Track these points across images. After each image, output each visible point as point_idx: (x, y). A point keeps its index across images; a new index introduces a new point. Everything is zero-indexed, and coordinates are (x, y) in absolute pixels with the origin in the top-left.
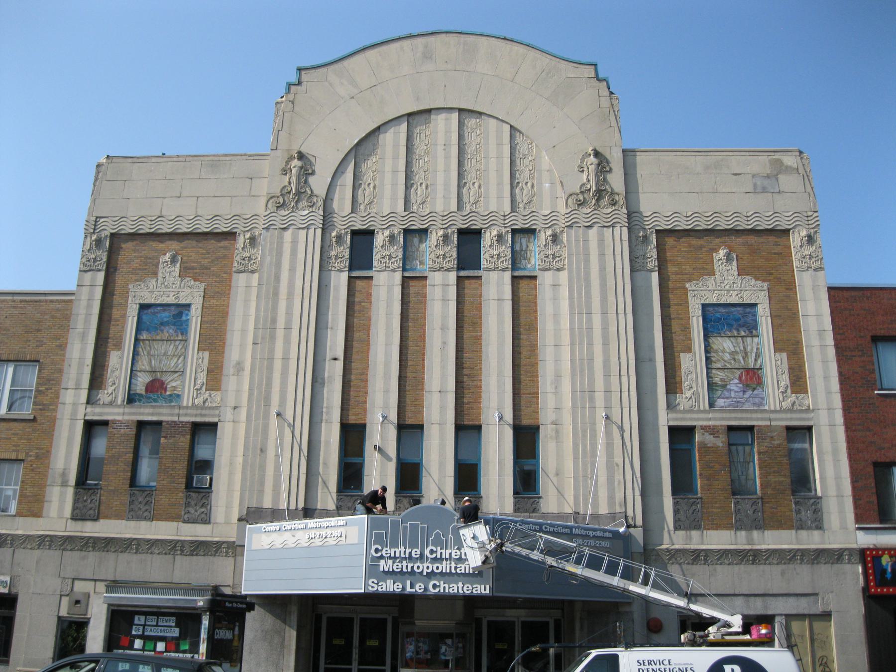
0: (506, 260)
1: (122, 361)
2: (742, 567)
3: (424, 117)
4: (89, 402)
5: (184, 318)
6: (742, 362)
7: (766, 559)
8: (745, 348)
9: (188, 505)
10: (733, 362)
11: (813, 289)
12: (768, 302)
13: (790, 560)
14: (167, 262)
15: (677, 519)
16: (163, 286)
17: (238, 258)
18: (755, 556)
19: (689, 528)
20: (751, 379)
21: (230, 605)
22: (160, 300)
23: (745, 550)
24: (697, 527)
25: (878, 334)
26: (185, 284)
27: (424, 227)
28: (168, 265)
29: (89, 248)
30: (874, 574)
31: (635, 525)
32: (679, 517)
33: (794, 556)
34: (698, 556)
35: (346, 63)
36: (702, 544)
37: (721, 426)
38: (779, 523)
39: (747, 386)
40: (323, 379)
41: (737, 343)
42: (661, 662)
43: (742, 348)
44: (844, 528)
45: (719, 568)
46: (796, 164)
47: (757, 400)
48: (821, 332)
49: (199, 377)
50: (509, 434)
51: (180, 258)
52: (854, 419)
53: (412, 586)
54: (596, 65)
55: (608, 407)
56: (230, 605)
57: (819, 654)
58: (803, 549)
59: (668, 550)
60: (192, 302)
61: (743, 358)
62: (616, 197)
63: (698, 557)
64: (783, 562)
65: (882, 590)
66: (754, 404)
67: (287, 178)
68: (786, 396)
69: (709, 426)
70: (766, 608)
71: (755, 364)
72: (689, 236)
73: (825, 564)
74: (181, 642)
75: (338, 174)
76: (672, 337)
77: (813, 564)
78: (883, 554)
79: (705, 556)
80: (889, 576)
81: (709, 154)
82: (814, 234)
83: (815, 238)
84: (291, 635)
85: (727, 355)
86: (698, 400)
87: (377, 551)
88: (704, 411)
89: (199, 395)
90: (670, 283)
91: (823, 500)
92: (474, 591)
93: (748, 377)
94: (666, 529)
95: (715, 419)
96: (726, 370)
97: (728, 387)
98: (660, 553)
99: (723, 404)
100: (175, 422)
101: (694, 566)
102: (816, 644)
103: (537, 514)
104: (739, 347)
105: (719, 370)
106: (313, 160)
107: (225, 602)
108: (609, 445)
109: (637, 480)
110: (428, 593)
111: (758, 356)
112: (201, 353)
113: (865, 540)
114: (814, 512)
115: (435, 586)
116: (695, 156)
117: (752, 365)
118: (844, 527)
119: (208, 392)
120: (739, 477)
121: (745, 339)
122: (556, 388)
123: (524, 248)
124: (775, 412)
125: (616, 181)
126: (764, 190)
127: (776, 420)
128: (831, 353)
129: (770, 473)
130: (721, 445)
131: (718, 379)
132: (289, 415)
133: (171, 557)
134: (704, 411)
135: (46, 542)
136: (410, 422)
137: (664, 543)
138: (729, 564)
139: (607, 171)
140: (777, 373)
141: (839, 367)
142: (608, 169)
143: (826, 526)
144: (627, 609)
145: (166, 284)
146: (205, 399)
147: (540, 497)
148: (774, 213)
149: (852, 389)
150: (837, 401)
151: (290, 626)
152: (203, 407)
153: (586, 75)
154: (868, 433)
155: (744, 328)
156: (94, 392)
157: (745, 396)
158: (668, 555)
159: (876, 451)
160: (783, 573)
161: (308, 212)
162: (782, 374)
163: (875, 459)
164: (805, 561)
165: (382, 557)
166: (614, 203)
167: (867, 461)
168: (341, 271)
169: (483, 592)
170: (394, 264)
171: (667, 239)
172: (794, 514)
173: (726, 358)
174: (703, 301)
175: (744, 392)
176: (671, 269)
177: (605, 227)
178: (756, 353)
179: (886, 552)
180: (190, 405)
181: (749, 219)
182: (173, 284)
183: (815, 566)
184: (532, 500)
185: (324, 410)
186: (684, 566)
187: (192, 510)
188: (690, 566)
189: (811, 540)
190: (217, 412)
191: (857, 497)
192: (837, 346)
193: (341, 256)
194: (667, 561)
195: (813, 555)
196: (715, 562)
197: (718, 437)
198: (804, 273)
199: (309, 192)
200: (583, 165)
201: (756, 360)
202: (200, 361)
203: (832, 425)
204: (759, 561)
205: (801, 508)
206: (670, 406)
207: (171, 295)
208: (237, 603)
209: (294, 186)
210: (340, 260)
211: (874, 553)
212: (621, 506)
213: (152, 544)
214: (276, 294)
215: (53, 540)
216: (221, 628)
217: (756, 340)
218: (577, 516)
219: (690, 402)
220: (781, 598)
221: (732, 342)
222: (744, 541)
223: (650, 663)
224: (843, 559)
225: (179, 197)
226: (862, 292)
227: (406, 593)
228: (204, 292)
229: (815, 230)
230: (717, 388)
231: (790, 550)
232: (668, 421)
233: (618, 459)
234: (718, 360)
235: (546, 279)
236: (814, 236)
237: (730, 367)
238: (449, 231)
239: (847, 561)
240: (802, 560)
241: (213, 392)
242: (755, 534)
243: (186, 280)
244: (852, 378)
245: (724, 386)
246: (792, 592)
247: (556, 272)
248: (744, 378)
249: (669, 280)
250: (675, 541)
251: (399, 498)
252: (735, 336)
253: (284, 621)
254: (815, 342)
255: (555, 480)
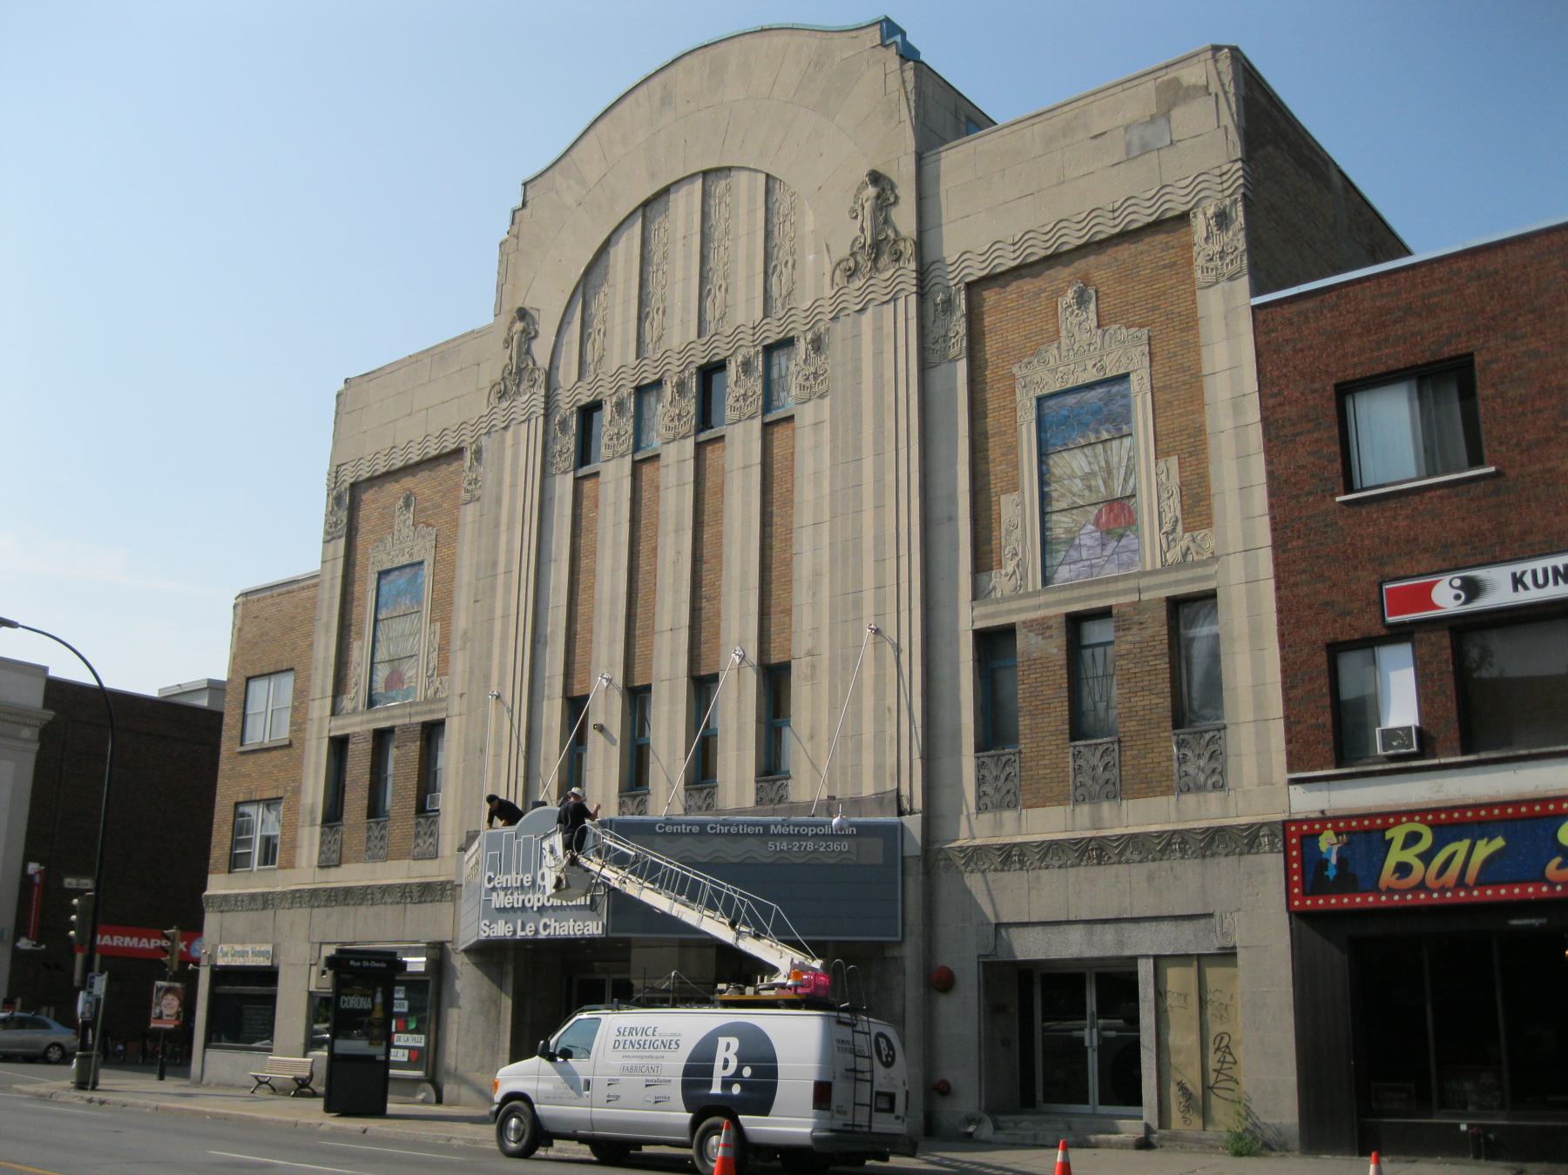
0: (1236, 257)
1: (363, 653)
2: (1081, 870)
3: (726, 172)
4: (335, 712)
5: (419, 581)
6: (1102, 489)
7: (1121, 854)
8: (1107, 462)
9: (417, 835)
10: (1086, 493)
11: (1225, 318)
12: (1148, 364)
13: (1163, 851)
14: (1070, 306)
15: (982, 794)
16: (1071, 353)
17: (1200, 261)
18: (1101, 849)
19: (1001, 806)
20: (1116, 517)
21: (358, 964)
22: (1071, 381)
23: (1083, 839)
24: (1012, 805)
25: (1349, 378)
26: (1111, 338)
27: (657, 376)
28: (1073, 312)
29: (1205, 235)
30: (1303, 871)
31: (911, 810)
32: (1082, 779)
33: (1169, 844)
34: (1009, 856)
35: (574, 153)
36: (1019, 833)
37: (1055, 616)
38: (1149, 786)
39: (1109, 532)
40: (546, 636)
41: (1096, 456)
42: (644, 1031)
43: (1103, 464)
44: (1265, 784)
45: (1044, 874)
46: (1204, 78)
47: (1124, 557)
48: (1237, 403)
49: (1167, 509)
50: (752, 679)
51: (1092, 292)
52: (1294, 562)
53: (523, 929)
54: (525, 184)
55: (879, 615)
56: (358, 964)
57: (1215, 1028)
58: (1182, 830)
59: (962, 849)
60: (1130, 368)
61: (1105, 482)
62: (901, 246)
63: (1010, 856)
64: (1150, 856)
65: (1327, 902)
66: (1120, 565)
67: (509, 351)
68: (1173, 540)
69: (1036, 620)
70: (1121, 944)
71: (1124, 489)
72: (1022, 277)
73: (1226, 855)
74: (409, 1019)
75: (565, 327)
76: (988, 469)
77: (1204, 856)
78: (1324, 828)
79: (1019, 855)
80: (1331, 873)
81: (1056, 112)
82: (1231, 206)
83: (1234, 215)
84: (507, 1003)
85: (1078, 481)
86: (1024, 577)
87: (490, 880)
88: (1036, 594)
89: (1172, 544)
90: (987, 373)
91: (1228, 731)
92: (586, 933)
93: (1112, 515)
94: (965, 813)
95: (1047, 605)
96: (1074, 511)
97: (1077, 541)
98: (951, 856)
99: (1067, 575)
100: (405, 725)
101: (1006, 874)
102: (1210, 1011)
103: (786, 805)
104: (1098, 463)
105: (1063, 513)
106: (536, 316)
107: (349, 960)
108: (879, 679)
109: (916, 732)
110: (540, 937)
111: (1130, 471)
112: (1162, 463)
113: (1307, 802)
114: (1211, 757)
115: (546, 926)
116: (1032, 125)
117: (1118, 493)
118: (1265, 781)
119: (1187, 535)
120: (1095, 706)
121: (1108, 444)
122: (814, 595)
123: (783, 374)
124: (1154, 572)
125: (904, 218)
126: (1146, 149)
127: (1149, 589)
128: (1255, 436)
129: (1136, 692)
130: (1055, 651)
131: (1061, 531)
132: (508, 698)
133: (402, 906)
134: (1036, 594)
135: (298, 898)
136: (638, 683)
137: (961, 836)
138: (1060, 867)
139: (891, 204)
140: (1159, 498)
141: (1269, 462)
142: (892, 200)
143: (1231, 782)
144: (895, 953)
145: (1076, 347)
146: (1184, 549)
147: (788, 778)
148: (1162, 188)
149: (1292, 503)
150: (1263, 532)
151: (506, 993)
152: (1183, 564)
153: (869, 45)
154: (1320, 586)
155: (1108, 426)
156: (983, 577)
157: (1105, 553)
158: (962, 858)
159: (1335, 621)
160: (1150, 878)
161: (893, 270)
162: (1169, 498)
163: (1332, 636)
164: (1190, 852)
165: (494, 889)
166: (898, 257)
167: (1314, 643)
168: (565, 472)
169: (596, 932)
170: (1232, 264)
171: (986, 294)
172: (1176, 765)
173: (1075, 489)
174: (1039, 393)
175: (1103, 545)
176: (991, 346)
177: (884, 303)
178: (1127, 467)
179: (1329, 825)
180: (1159, 566)
181: (1116, 214)
182: (1090, 344)
183: (1208, 860)
184: (778, 783)
185: (546, 681)
186: (990, 876)
187: (420, 841)
188: (1000, 874)
189: (1204, 811)
190: (445, 704)
191: (1292, 719)
192: (1265, 421)
193: (1230, 251)
194: (963, 868)
195: (1201, 841)
196: (1037, 864)
197: (1051, 636)
198: (1211, 290)
199: (531, 365)
200: (856, 206)
201: (1126, 481)
202: (1163, 477)
203: (1252, 581)
204: (1110, 858)
205: (1190, 754)
206: (976, 595)
207: (1089, 367)
208: (369, 961)
209: (868, 234)
210: (1230, 257)
211: (1537, 808)
212: (892, 781)
213: (386, 890)
214: (497, 525)
215: (1186, 837)
216: (351, 995)
217: (1127, 442)
218: (832, 802)
219: (1013, 581)
220: (1147, 925)
221: (1086, 457)
222: (1087, 824)
223: (631, 1033)
224: (1260, 844)
225: (409, 415)
226: (1320, 298)
227: (518, 937)
228: (1149, 344)
229: (1233, 198)
230: (1059, 547)
231: (1160, 834)
232: (973, 622)
233: (891, 701)
234: (1063, 495)
235: (806, 416)
236: (1230, 211)
237: (1082, 503)
238: (687, 373)
239: (1267, 848)
240: (1183, 851)
241: (1198, 532)
242: (1106, 808)
243: (1111, 331)
244: (1293, 480)
245: (1070, 542)
246: (1165, 913)
247: (819, 400)
248: (1104, 518)
249: (986, 368)
250: (976, 832)
251: (982, 759)
252: (1090, 444)
253: (500, 987)
254: (1226, 423)
255: (808, 745)
